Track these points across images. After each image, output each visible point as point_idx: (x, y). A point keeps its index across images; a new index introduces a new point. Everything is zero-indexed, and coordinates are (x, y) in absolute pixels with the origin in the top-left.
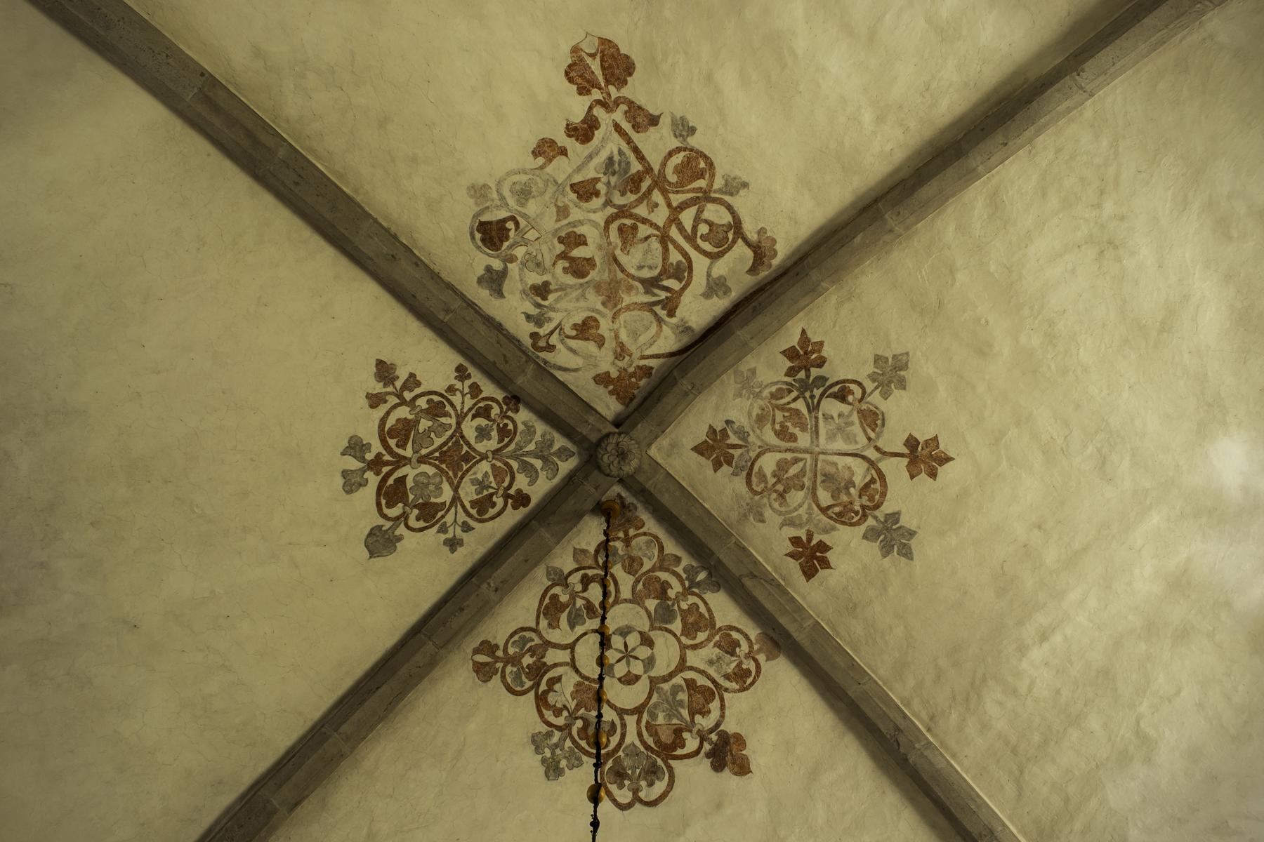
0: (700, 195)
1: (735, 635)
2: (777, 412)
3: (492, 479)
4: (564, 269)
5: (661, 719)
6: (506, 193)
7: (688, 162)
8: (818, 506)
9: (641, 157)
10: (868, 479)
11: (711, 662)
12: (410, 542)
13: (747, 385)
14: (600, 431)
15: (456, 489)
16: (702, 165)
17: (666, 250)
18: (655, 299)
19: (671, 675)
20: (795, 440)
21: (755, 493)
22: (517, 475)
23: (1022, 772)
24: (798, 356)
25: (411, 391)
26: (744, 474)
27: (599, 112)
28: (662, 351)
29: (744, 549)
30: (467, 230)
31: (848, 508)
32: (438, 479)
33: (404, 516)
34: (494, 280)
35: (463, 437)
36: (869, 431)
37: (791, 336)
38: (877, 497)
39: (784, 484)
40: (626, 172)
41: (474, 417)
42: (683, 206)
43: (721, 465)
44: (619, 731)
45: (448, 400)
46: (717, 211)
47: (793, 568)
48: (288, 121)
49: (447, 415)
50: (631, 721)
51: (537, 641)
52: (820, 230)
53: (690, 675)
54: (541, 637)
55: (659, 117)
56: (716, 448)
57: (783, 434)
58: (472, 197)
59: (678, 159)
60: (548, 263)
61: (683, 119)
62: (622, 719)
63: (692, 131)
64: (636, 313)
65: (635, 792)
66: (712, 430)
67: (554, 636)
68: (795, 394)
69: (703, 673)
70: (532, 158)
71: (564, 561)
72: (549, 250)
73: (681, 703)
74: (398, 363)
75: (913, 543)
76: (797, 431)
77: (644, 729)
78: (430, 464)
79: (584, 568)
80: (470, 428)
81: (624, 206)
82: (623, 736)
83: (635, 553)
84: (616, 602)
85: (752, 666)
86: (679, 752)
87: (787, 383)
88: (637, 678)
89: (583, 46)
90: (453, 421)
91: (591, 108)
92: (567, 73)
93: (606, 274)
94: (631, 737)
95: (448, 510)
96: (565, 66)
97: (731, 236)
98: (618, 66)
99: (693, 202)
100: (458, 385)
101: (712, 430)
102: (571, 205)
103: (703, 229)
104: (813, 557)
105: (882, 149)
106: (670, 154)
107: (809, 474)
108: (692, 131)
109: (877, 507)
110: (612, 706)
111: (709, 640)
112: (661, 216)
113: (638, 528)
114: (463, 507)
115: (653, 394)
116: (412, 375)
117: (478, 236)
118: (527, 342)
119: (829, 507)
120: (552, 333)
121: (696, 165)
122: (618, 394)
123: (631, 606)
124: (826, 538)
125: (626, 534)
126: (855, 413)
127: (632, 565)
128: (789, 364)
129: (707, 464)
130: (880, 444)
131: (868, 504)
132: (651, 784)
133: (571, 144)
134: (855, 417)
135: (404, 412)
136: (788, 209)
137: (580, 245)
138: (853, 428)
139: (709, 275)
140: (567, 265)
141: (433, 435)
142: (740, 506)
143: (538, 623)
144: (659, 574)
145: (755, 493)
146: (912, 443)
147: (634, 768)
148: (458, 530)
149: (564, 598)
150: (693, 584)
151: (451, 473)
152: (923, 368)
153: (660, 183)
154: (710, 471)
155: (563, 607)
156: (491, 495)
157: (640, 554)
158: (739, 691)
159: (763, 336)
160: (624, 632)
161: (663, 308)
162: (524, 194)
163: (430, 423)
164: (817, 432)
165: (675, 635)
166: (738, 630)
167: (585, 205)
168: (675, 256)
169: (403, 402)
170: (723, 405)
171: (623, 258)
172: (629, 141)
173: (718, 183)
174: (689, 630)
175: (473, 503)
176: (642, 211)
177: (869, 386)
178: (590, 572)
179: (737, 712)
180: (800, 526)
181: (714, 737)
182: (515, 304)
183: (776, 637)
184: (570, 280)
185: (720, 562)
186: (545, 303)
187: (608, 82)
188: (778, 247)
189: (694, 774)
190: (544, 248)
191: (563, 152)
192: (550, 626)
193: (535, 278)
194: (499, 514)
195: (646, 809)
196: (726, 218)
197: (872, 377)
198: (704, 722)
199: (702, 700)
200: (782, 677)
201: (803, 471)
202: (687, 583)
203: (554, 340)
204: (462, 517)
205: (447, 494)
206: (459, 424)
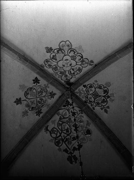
9: (66, 144)
15: (95, 90)
16: (56, 144)
19: (59, 61)
27: (73, 152)
33: (104, 88)
34: (88, 124)
35: (94, 98)
37: (41, 115)
41: (92, 101)
42: (59, 136)
47: (39, 78)
56: (52, 95)
57: (42, 99)
65: (66, 43)
66: (53, 98)
69: (53, 61)
72: (80, 129)
77: (64, 52)
80: (93, 100)
82: (68, 52)
85: (45, 63)
86: (58, 50)
88: (65, 60)
90: (95, 101)
91: (74, 153)
100: (94, 107)
101: (53, 98)
103: (56, 133)
106: (61, 145)
107: (37, 94)
110: (70, 56)
112: (63, 134)
118: (83, 112)
120: (79, 114)
124: (34, 84)
130: (26, 101)
135: (104, 104)
139: (55, 124)
146: (21, 103)
148: (95, 83)
153: (63, 140)
156: (90, 88)
169: (103, 106)
172: (68, 147)
175: (93, 87)
177: (28, 111)
178: (73, 75)
186: (80, 119)
193: (82, 124)
194: (88, 85)
197: (28, 112)
198: (54, 54)
203: (79, 112)
204: (94, 85)
206: (94, 101)
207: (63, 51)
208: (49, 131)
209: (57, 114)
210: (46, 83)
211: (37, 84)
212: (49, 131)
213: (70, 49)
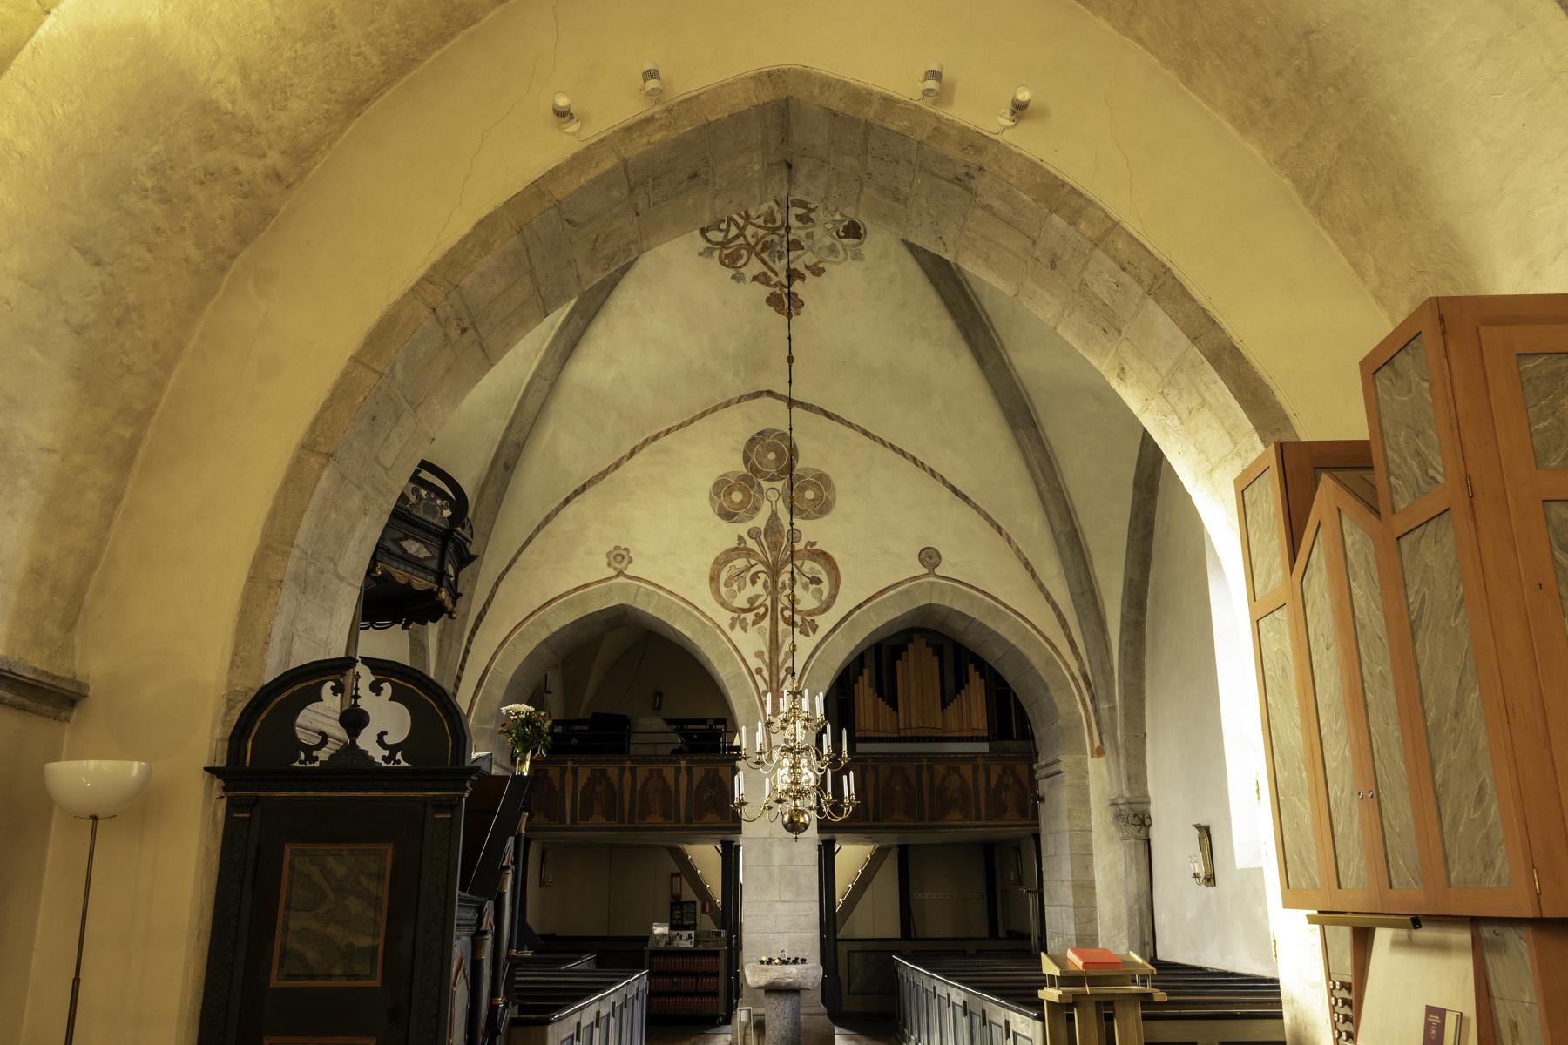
42: (737, 237)
103: (723, 226)
112: (750, 230)
121: (731, 261)
133: (803, 270)
153: (751, 249)
162: (832, 250)
173: (716, 254)
176: (761, 232)
191: (807, 267)
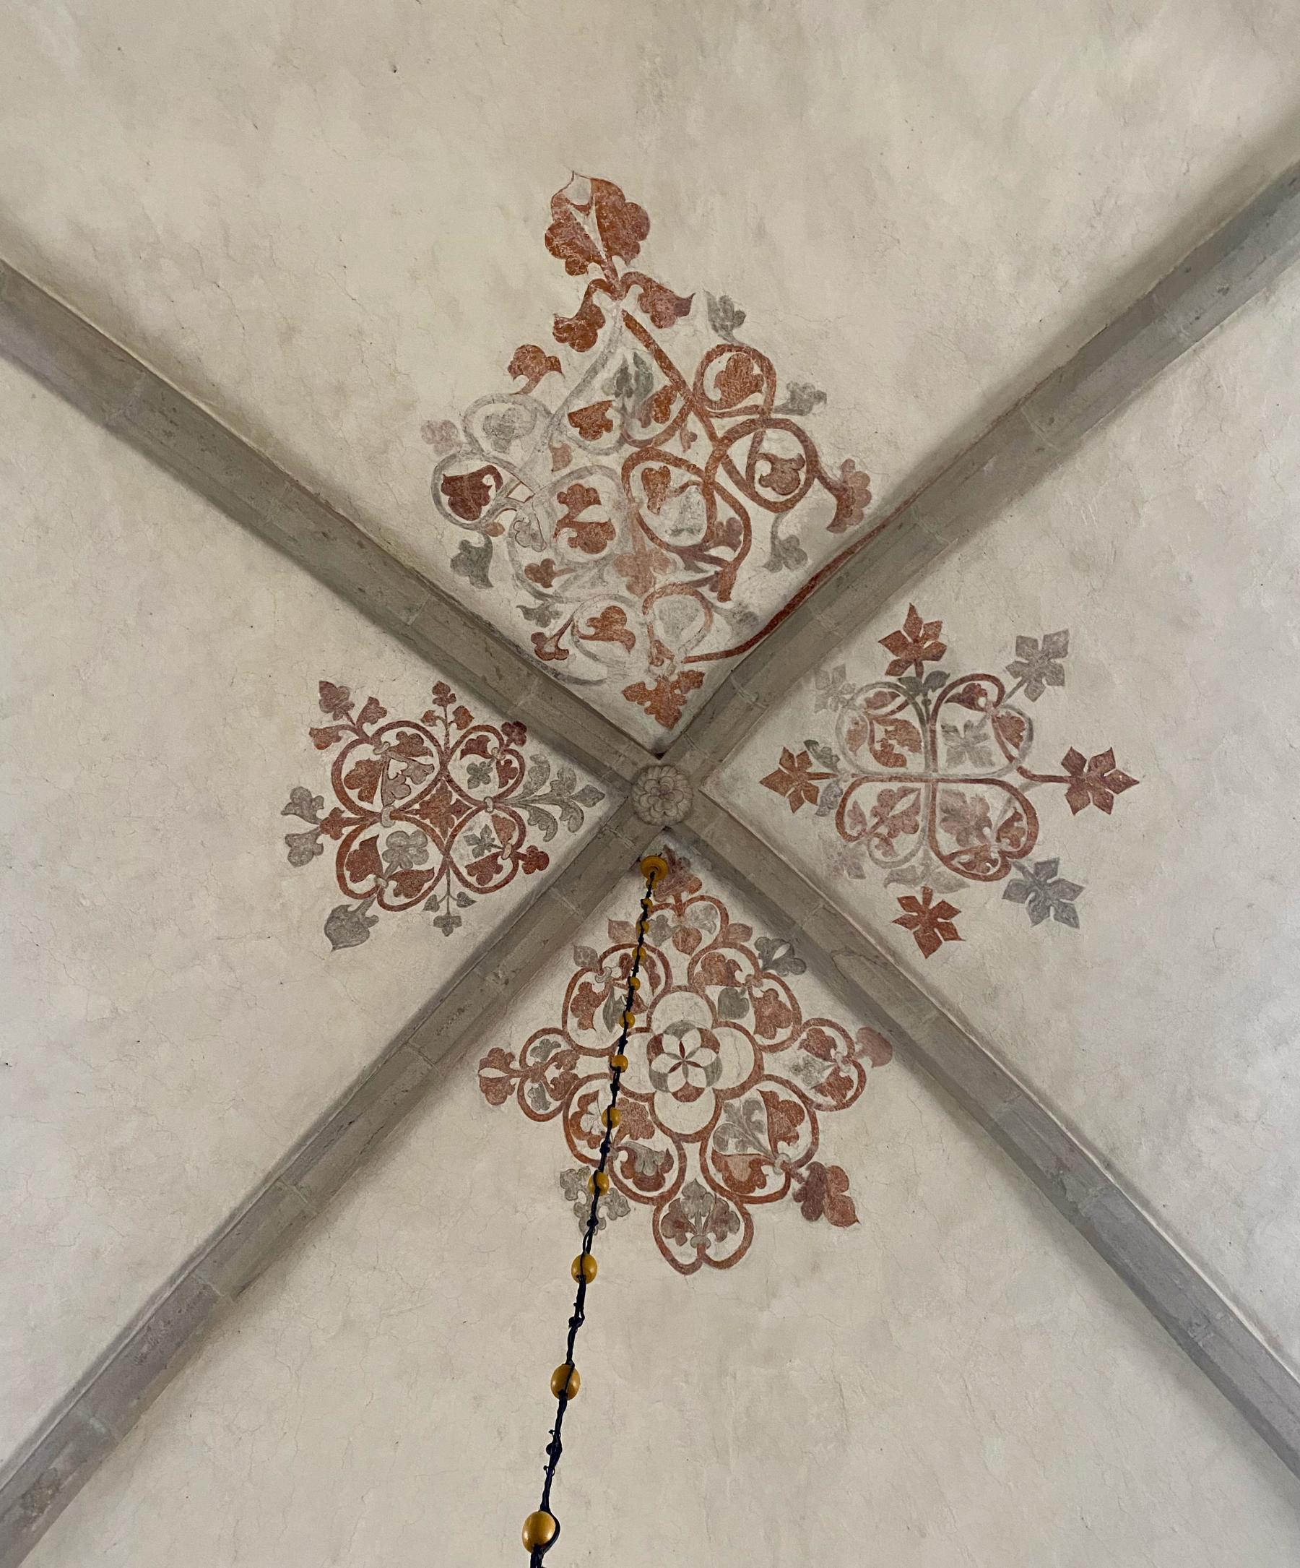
0: (756, 417)
1: (828, 1031)
2: (876, 726)
3: (494, 835)
4: (571, 540)
5: (731, 1149)
6: (478, 433)
7: (735, 368)
8: (938, 854)
9: (667, 367)
10: (1009, 814)
11: (797, 1069)
12: (387, 924)
13: (837, 694)
14: (634, 764)
15: (446, 851)
17: (711, 504)
18: (700, 576)
19: (744, 1087)
20: (904, 764)
21: (851, 839)
22: (528, 828)
23: (1251, 1232)
24: (905, 644)
25: (373, 722)
26: (834, 812)
27: (600, 299)
28: (714, 650)
29: (836, 915)
30: (428, 491)
31: (981, 856)
32: (421, 840)
33: (378, 891)
34: (475, 562)
35: (450, 781)
36: (1010, 747)
37: (894, 620)
38: (1024, 839)
39: (889, 824)
40: (647, 390)
41: (463, 754)
42: (732, 436)
43: (801, 803)
44: (676, 1165)
45: (426, 733)
46: (781, 440)
47: (905, 941)
48: (145, 339)
49: (427, 752)
50: (692, 1150)
51: (565, 1046)
52: (933, 455)
53: (769, 1086)
54: (570, 1041)
55: (689, 300)
56: (794, 778)
57: (885, 756)
58: (429, 441)
59: (720, 364)
60: (547, 532)
61: (724, 300)
62: (680, 1148)
63: (739, 318)
64: (675, 597)
65: (701, 1248)
66: (788, 755)
67: (587, 1039)
68: (901, 700)
70: (509, 377)
71: (599, 940)
72: (546, 514)
73: (758, 1125)
74: (352, 685)
75: (1078, 903)
76: (905, 751)
77: (709, 1162)
78: (408, 820)
79: (623, 947)
80: (459, 769)
81: (649, 441)
82: (682, 1171)
83: (690, 924)
84: (666, 991)
86: (758, 1193)
87: (889, 685)
88: (699, 1092)
89: (569, 194)
90: (435, 761)
91: (588, 294)
92: (548, 241)
93: (630, 544)
94: (693, 1173)
95: (438, 879)
96: (544, 231)
97: (803, 476)
98: (624, 224)
99: (748, 427)
100: (439, 711)
101: (788, 755)
102: (572, 445)
103: (763, 468)
104: (934, 924)
105: (1026, 316)
106: (709, 358)
107: (924, 810)
108: (739, 318)
109: (1024, 853)
110: (666, 1131)
111: (792, 1038)
112: (701, 453)
113: (692, 891)
114: (458, 874)
115: (708, 709)
116: (373, 701)
117: (445, 499)
118: (529, 647)
119: (953, 855)
120: (561, 632)
121: (747, 370)
122: (658, 713)
123: (687, 994)
124: (950, 898)
125: (678, 899)
126: (989, 722)
127: (686, 940)
128: (892, 657)
129: (781, 801)
130: (1026, 765)
131: (1010, 849)
132: (721, 1238)
134: (989, 729)
135: (365, 752)
136: (884, 427)
137: (590, 503)
138: (986, 743)
139: (774, 536)
140: (574, 535)
141: (408, 781)
142: (830, 857)
143: (565, 1022)
144: (722, 951)
145: (851, 839)
146: (1073, 761)
147: (698, 1216)
148: (453, 904)
149: (598, 988)
150: (769, 963)
151: (437, 830)
152: (1087, 650)
153: (697, 403)
154: (786, 811)
155: (597, 1000)
156: (495, 856)
157: (696, 925)
158: (837, 1108)
159: (855, 623)
160: (679, 1030)
161: (712, 590)
162: (503, 432)
163: (404, 765)
164: (934, 752)
165: (747, 1033)
166: (832, 1025)
167: (591, 444)
168: (725, 513)
169: (364, 739)
170: (810, 719)
171: (651, 520)
172: (649, 342)
174: (767, 1025)
175: (471, 869)
176: (673, 447)
177: (1009, 682)
179: (836, 1138)
180: (913, 882)
181: (804, 1172)
182: (507, 595)
183: (885, 1034)
184: (580, 556)
185: (803, 933)
186: (549, 591)
187: (610, 251)
188: (873, 488)
189: (778, 1221)
190: (540, 512)
191: (555, 365)
192: (581, 1025)
193: (531, 557)
194: (507, 881)
195: (716, 1271)
196: (794, 449)
197: (1014, 670)
199: (786, 1122)
200: (893, 1092)
201: (915, 807)
202: (761, 962)
203: (565, 642)
204: (457, 887)
205: (434, 859)
206: (443, 764)
207: (719, 1178)
208: (824, 480)
209: (751, 614)
210: (848, 888)
211: (927, 901)
212: (824, 480)
213: (663, 1199)
